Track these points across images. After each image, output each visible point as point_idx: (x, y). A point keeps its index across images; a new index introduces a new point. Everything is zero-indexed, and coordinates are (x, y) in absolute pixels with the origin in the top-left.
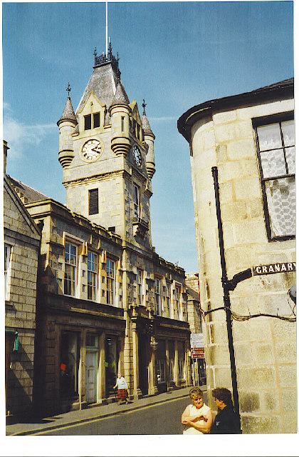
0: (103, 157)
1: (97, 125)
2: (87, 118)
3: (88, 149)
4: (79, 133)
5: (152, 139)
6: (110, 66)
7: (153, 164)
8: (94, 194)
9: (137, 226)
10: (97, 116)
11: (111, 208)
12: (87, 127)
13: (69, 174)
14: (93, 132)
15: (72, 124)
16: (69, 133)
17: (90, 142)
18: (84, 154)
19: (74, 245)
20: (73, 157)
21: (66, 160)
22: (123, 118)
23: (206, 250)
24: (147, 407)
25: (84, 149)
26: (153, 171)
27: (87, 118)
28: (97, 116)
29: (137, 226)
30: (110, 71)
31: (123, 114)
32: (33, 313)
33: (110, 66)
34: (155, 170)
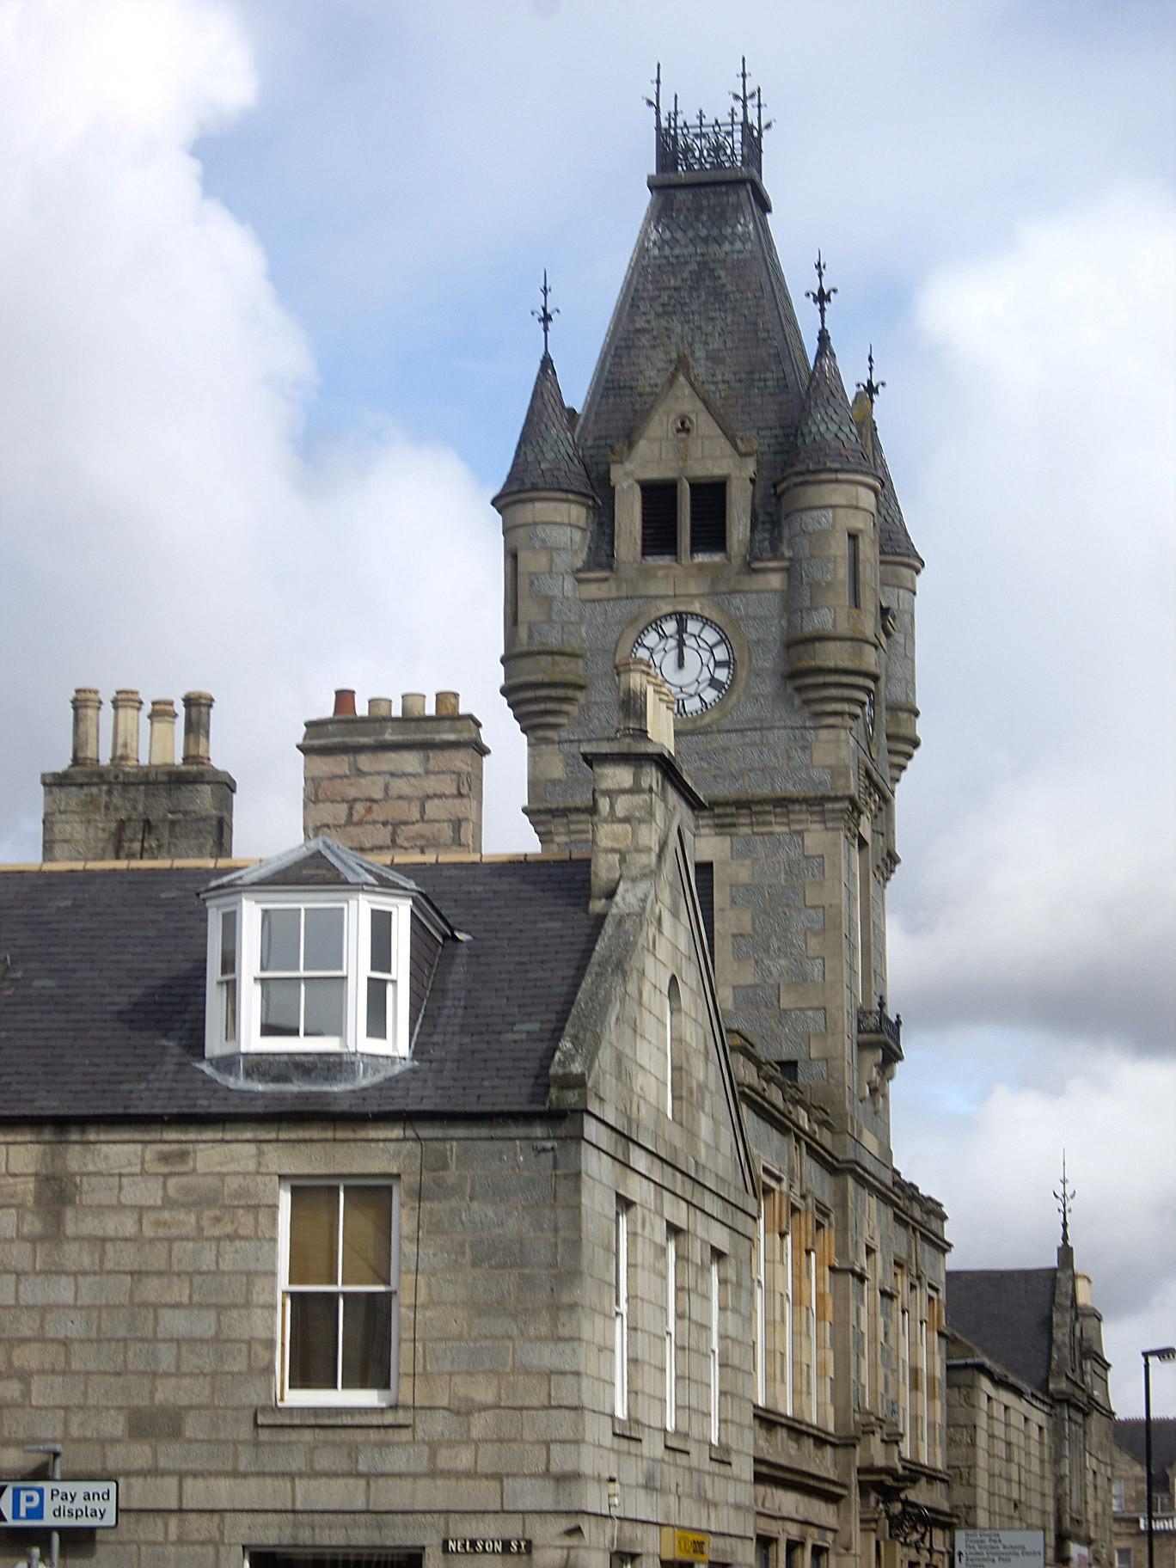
10: (711, 495)
27: (658, 496)
28: (711, 495)
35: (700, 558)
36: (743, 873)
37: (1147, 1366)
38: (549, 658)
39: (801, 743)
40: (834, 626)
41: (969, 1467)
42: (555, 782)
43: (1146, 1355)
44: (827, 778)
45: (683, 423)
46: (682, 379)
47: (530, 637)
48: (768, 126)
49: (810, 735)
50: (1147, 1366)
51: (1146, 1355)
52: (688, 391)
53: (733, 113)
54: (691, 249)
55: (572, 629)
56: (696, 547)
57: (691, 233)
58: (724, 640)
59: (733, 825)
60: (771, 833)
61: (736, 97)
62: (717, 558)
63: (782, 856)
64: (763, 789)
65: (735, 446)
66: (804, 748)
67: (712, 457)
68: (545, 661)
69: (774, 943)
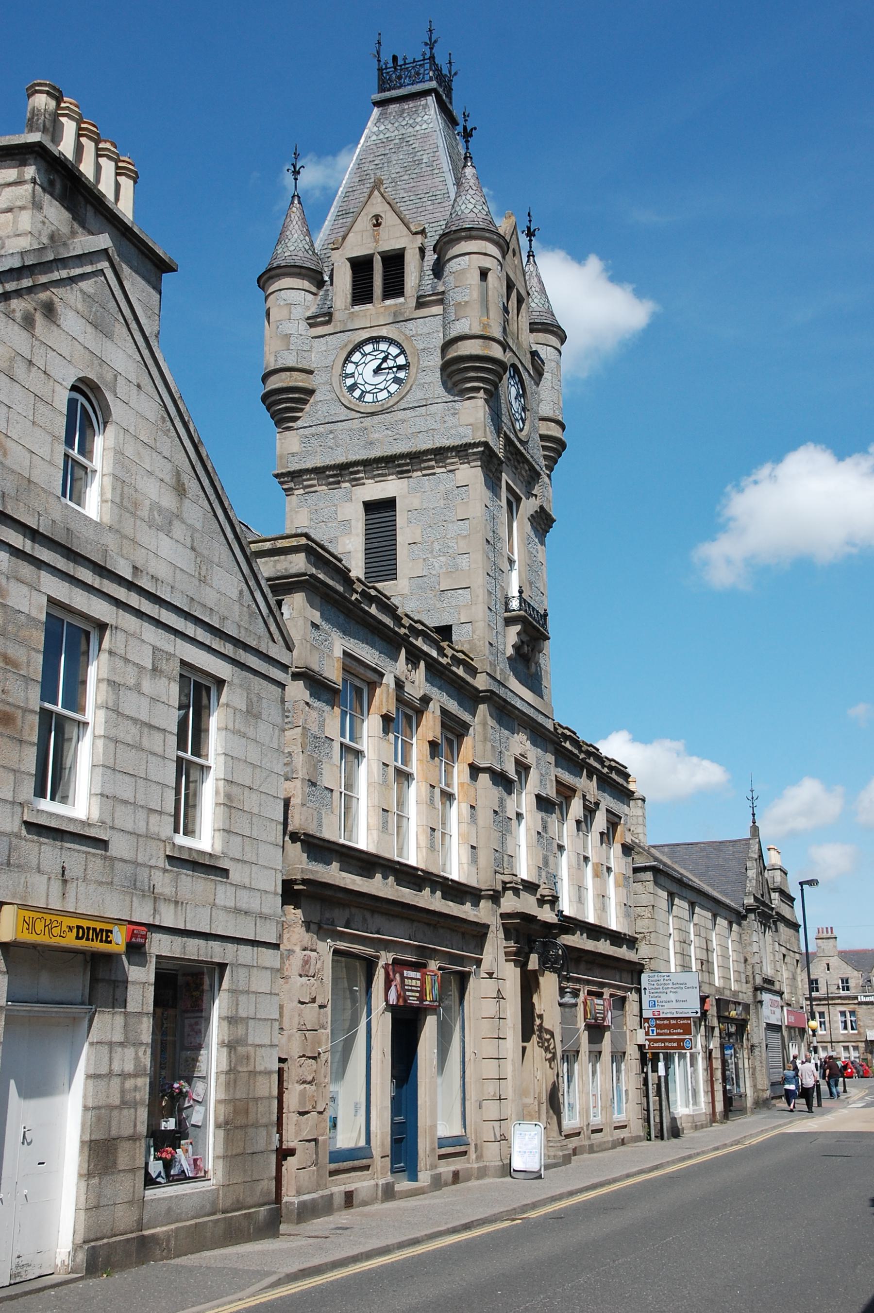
0: (416, 396)
1: (394, 287)
2: (361, 267)
3: (364, 370)
4: (330, 315)
5: (554, 340)
6: (431, 100)
7: (563, 426)
8: (381, 510)
9: (518, 628)
10: (394, 261)
11: (439, 563)
12: (362, 294)
13: (293, 447)
14: (376, 314)
15: (306, 284)
16: (300, 313)
17: (368, 348)
18: (350, 382)
19: (358, 683)
20: (311, 392)
21: (285, 404)
22: (484, 274)
23: (117, 773)
24: (592, 1194)
25: (350, 368)
26: (556, 448)
27: (361, 267)
28: (394, 261)
29: (518, 628)
30: (428, 117)
31: (487, 263)
32: (276, 894)
33: (431, 100)
34: (563, 445)
35: (388, 302)
36: (416, 503)
37: (802, 890)
38: (288, 373)
39: (452, 411)
40: (470, 329)
41: (302, 872)
42: (293, 455)
43: (801, 884)
44: (469, 432)
45: (377, 220)
46: (376, 192)
47: (276, 361)
48: (456, 74)
49: (457, 405)
50: (802, 890)
51: (801, 884)
52: (380, 199)
53: (424, 54)
54: (396, 133)
55: (306, 354)
56: (386, 295)
57: (396, 125)
58: (403, 352)
59: (408, 471)
60: (434, 474)
61: (426, 44)
62: (402, 300)
63: (442, 488)
64: (425, 444)
65: (409, 229)
66: (454, 414)
67: (394, 237)
68: (284, 375)
69: (436, 546)
